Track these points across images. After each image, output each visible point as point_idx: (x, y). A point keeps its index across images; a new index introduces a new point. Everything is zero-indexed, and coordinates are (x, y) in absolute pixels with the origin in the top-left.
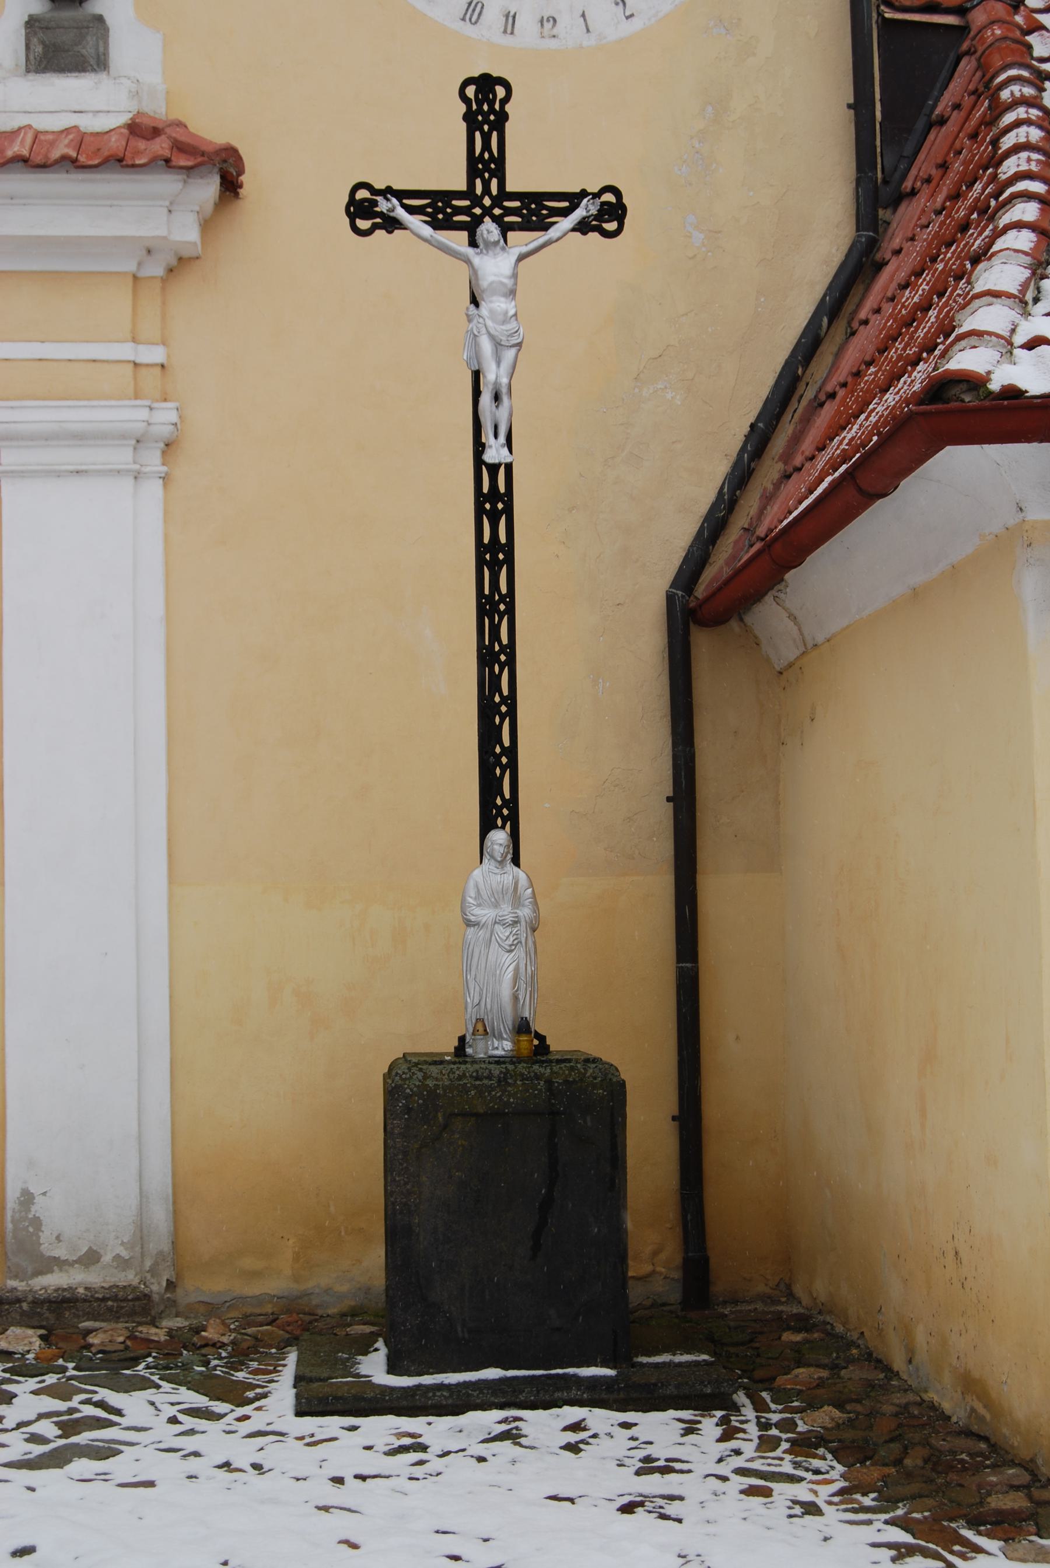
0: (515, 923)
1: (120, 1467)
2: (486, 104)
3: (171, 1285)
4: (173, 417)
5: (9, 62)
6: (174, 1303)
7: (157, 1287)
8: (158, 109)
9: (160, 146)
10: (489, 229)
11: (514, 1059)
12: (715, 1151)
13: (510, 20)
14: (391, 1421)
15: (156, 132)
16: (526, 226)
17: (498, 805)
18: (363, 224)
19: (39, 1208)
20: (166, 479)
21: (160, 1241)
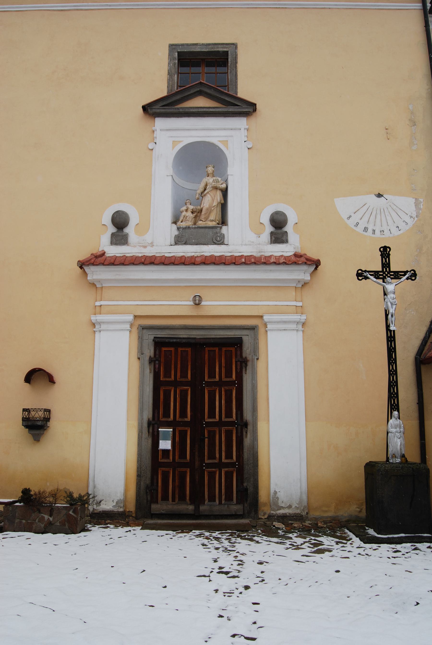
0: (400, 432)
2: (385, 252)
4: (305, 318)
5: (267, 241)
6: (307, 517)
7: (304, 514)
8: (299, 251)
9: (303, 259)
11: (400, 463)
13: (374, 231)
15: (301, 256)
18: (360, 278)
19: (278, 495)
20: (303, 331)
21: (305, 503)
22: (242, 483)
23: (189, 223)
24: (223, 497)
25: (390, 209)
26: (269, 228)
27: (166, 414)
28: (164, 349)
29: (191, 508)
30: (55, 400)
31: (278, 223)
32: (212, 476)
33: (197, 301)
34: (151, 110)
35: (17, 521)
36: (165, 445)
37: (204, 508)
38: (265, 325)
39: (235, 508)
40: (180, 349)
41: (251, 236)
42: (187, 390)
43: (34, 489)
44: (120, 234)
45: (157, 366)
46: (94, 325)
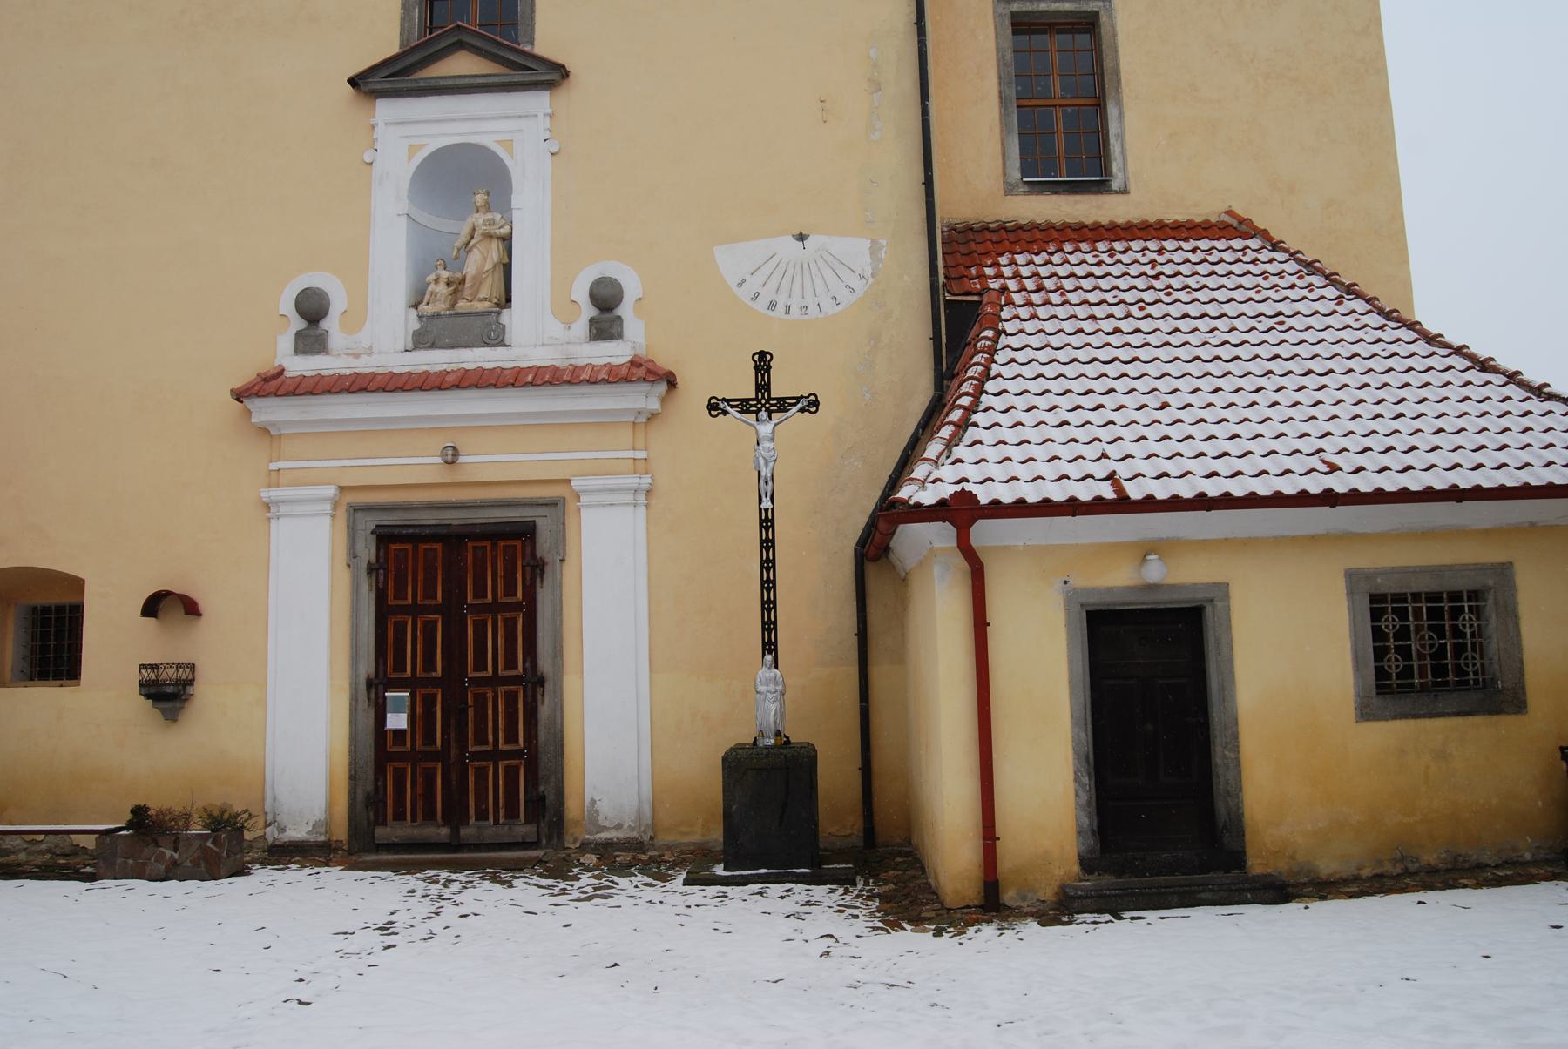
1: (610, 902)
2: (762, 362)
3: (652, 838)
7: (646, 839)
8: (643, 352)
9: (641, 372)
10: (763, 414)
11: (772, 747)
12: (877, 784)
13: (788, 308)
14: (719, 888)
16: (779, 411)
17: (770, 646)
21: (647, 819)
22: (536, 786)
23: (441, 306)
24: (502, 812)
25: (821, 264)
26: (588, 311)
27: (400, 665)
28: (394, 547)
29: (445, 831)
30: (204, 647)
31: (606, 300)
32: (481, 774)
33: (452, 457)
34: (374, 83)
35: (119, 861)
36: (397, 721)
37: (468, 832)
38: (578, 498)
39: (523, 830)
40: (422, 546)
41: (555, 329)
42: (436, 621)
43: (154, 805)
44: (312, 332)
45: (381, 578)
46: (267, 506)
